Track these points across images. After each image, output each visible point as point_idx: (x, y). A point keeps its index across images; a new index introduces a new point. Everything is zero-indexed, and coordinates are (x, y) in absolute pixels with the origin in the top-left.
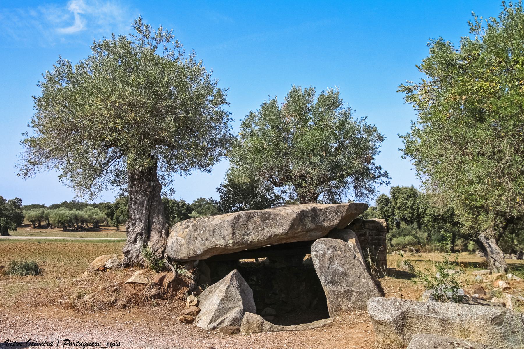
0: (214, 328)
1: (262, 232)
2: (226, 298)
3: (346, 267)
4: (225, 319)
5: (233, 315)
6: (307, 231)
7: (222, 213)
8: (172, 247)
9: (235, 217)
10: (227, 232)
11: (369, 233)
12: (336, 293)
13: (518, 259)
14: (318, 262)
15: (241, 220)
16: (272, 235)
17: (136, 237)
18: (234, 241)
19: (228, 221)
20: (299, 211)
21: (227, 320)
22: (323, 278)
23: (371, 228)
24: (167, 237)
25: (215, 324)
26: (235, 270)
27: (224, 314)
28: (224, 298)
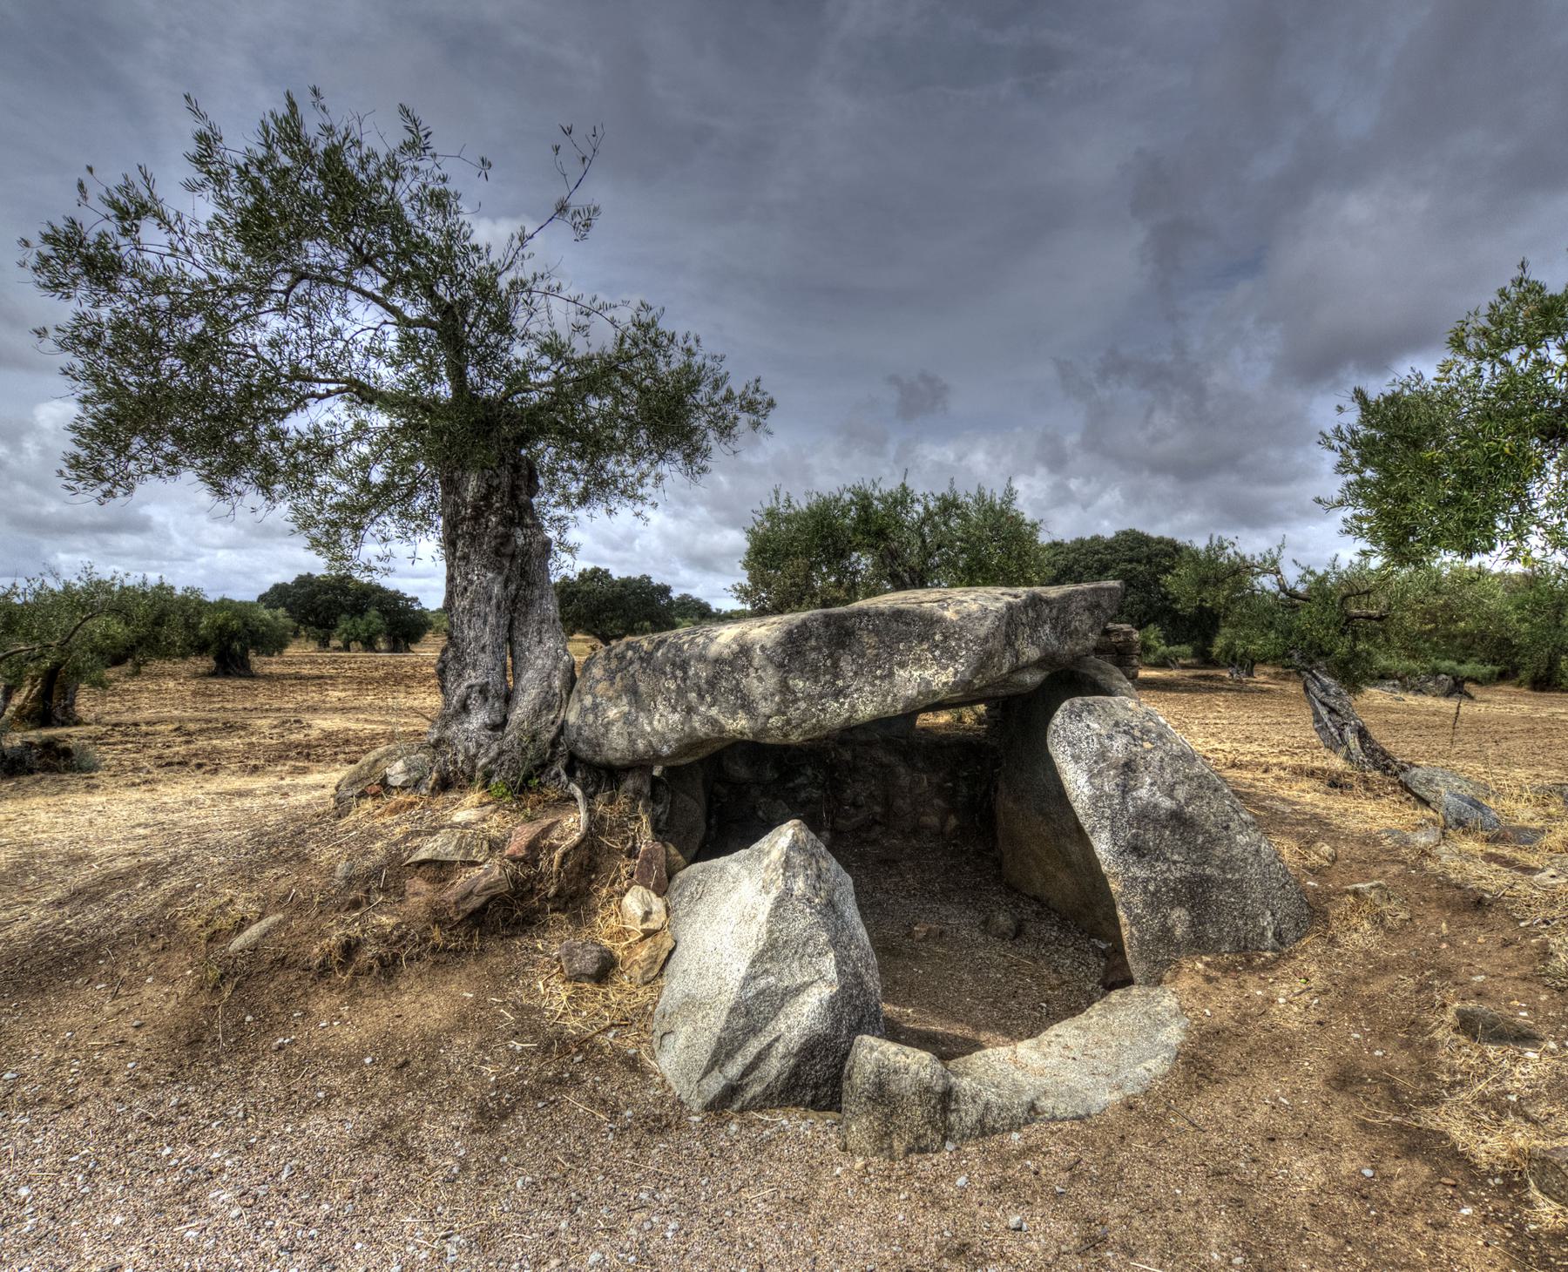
0: (732, 1091)
1: (886, 685)
3: (1181, 793)
4: (770, 1046)
5: (805, 1022)
7: (978, 585)
8: (579, 728)
9: (790, 633)
12: (1151, 888)
14: (1082, 780)
19: (763, 648)
21: (780, 1048)
22: (1105, 835)
24: (569, 693)
25: (733, 1069)
27: (767, 1020)
28: (763, 952)
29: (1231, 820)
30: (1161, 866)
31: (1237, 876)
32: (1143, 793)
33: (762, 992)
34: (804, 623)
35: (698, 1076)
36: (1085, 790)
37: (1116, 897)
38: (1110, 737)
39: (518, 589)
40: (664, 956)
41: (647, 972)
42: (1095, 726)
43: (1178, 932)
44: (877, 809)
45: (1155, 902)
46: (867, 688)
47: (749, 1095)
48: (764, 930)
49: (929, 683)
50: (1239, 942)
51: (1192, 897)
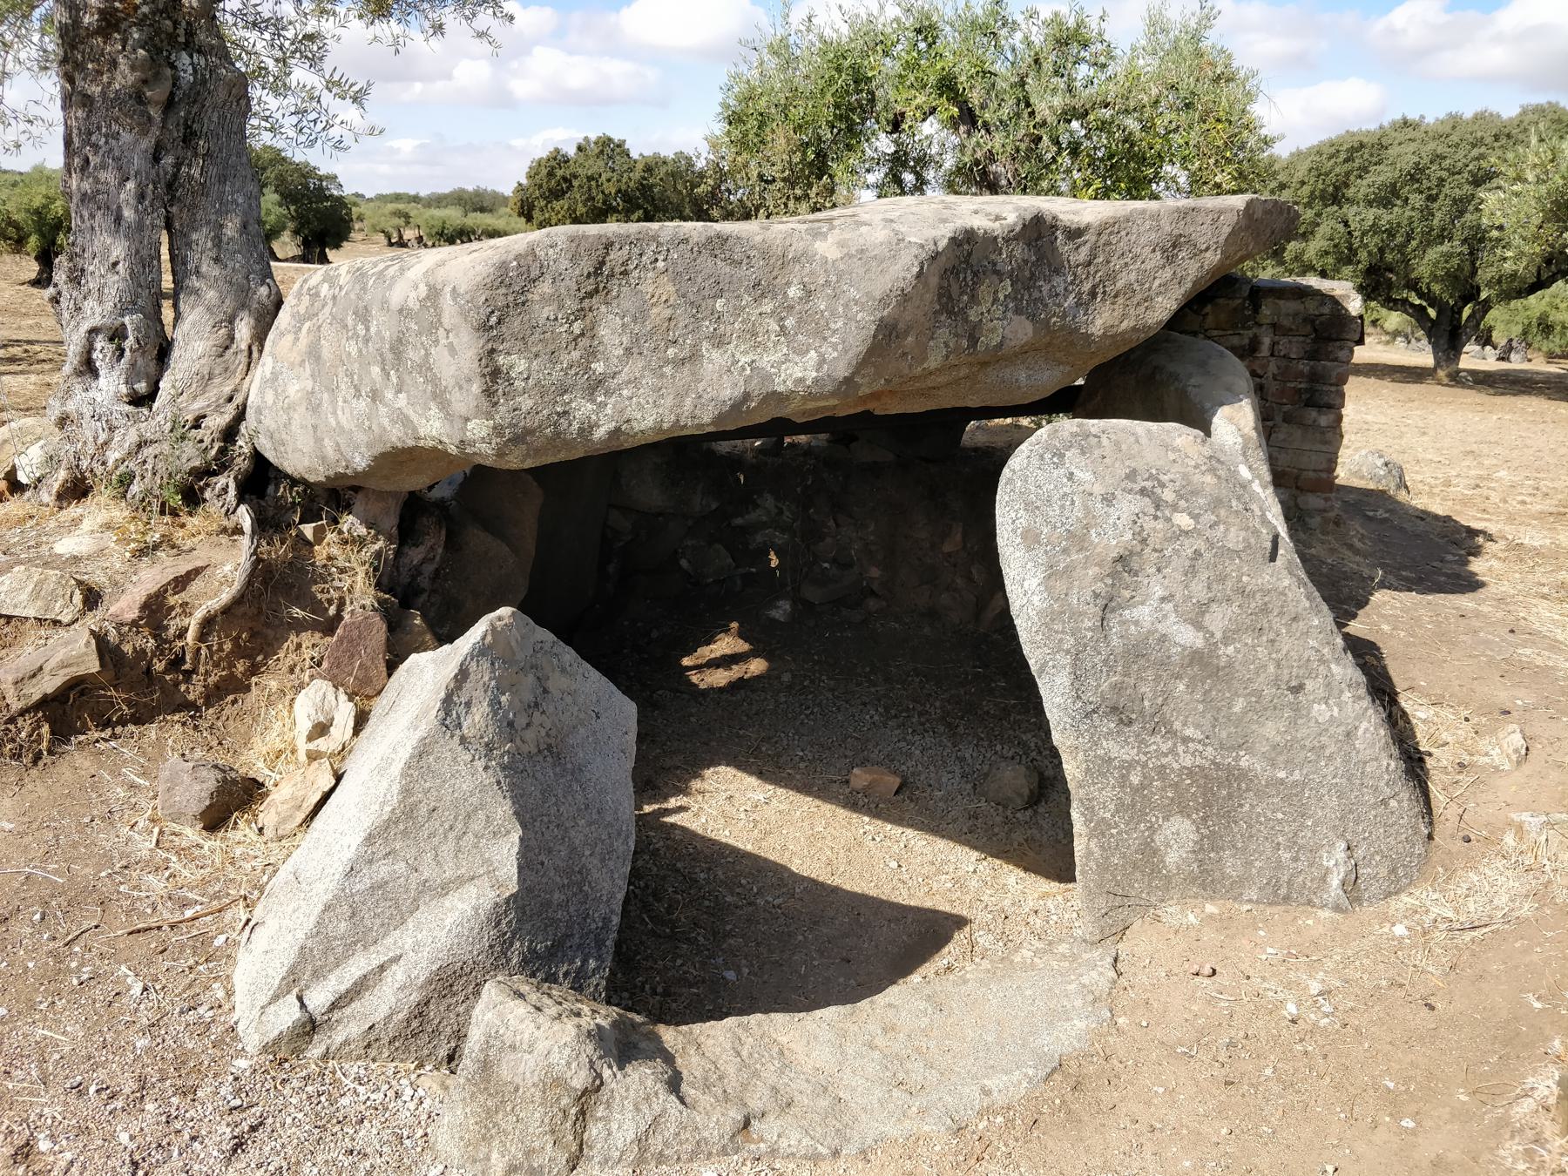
2: (401, 824)
3: (1218, 620)
6: (984, 364)
9: (503, 266)
10: (456, 356)
11: (1274, 344)
12: (1135, 779)
13: (1501, 359)
15: (545, 287)
16: (746, 396)
17: (90, 349)
18: (498, 430)
20: (944, 233)
21: (397, 975)
23: (1286, 322)
26: (505, 611)
27: (386, 928)
28: (388, 825)
29: (1313, 675)
30: (1159, 743)
31: (1297, 776)
32: (1143, 613)
33: (382, 885)
34: (532, 252)
35: (264, 1000)
36: (1036, 599)
37: (1071, 786)
38: (1108, 499)
39: (178, 166)
40: (317, 797)
41: (284, 820)
42: (1084, 476)
43: (1172, 858)
44: (875, 572)
45: (1136, 805)
46: (649, 380)
47: (339, 1038)
48: (396, 788)
49: (768, 378)
50: (1277, 887)
51: (1207, 804)
